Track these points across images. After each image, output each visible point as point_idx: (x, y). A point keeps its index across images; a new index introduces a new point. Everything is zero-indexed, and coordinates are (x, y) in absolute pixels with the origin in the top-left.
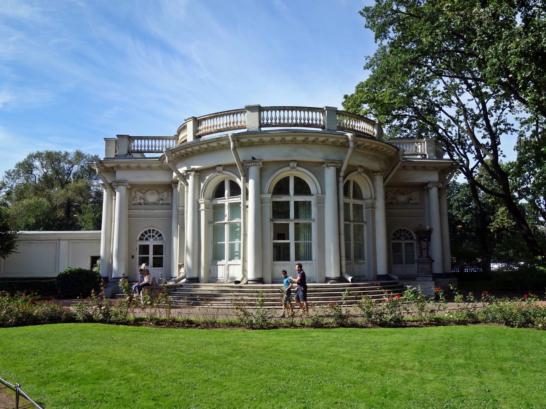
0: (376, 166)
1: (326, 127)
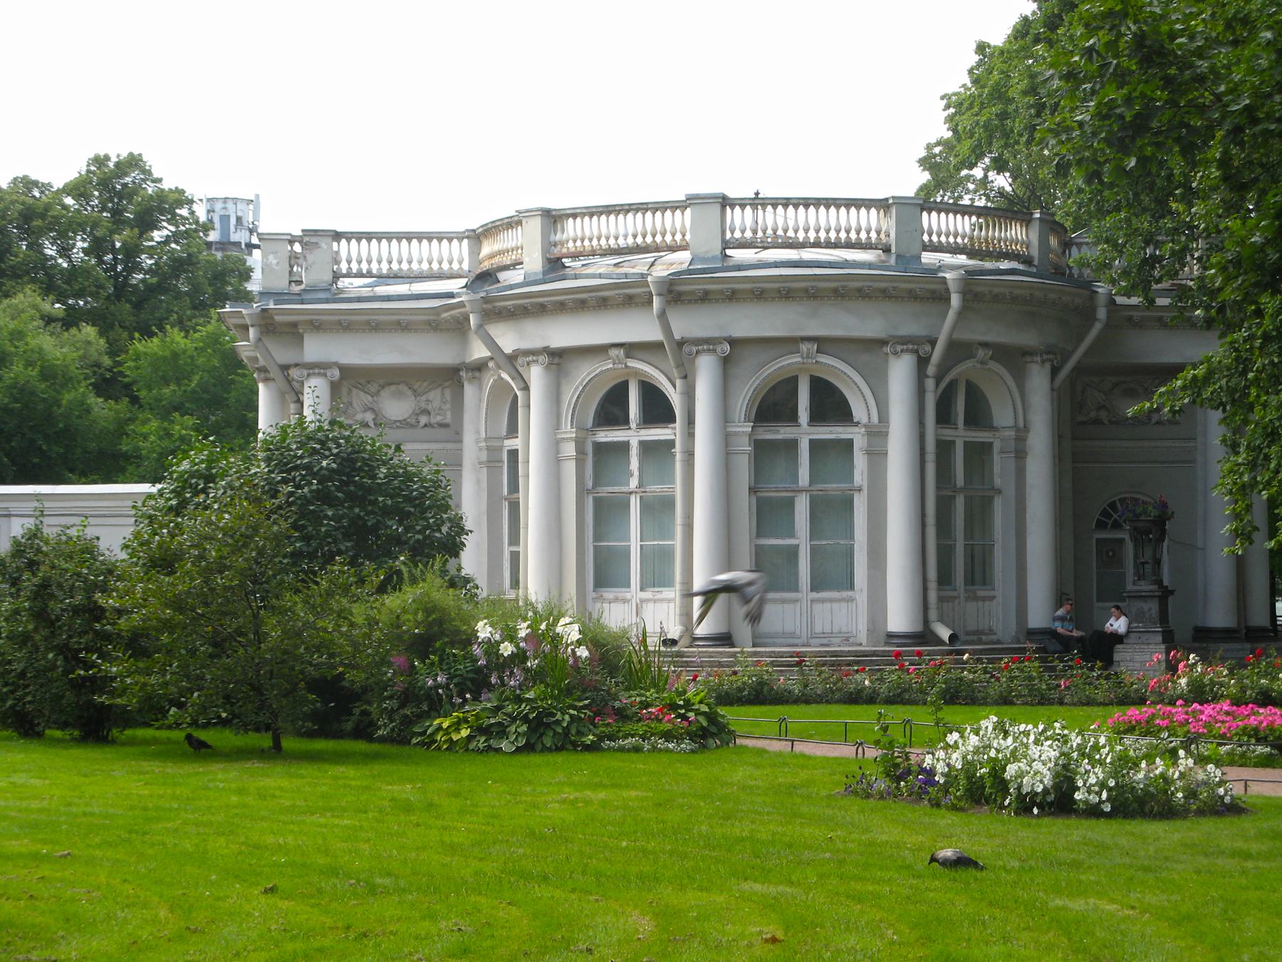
0: (1028, 338)
1: (893, 250)
